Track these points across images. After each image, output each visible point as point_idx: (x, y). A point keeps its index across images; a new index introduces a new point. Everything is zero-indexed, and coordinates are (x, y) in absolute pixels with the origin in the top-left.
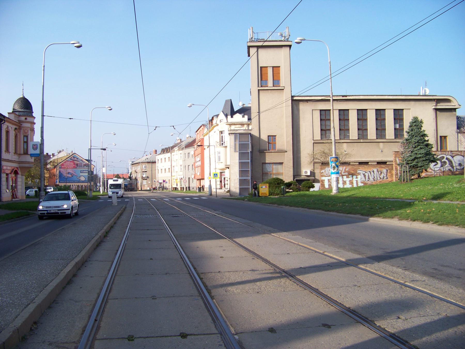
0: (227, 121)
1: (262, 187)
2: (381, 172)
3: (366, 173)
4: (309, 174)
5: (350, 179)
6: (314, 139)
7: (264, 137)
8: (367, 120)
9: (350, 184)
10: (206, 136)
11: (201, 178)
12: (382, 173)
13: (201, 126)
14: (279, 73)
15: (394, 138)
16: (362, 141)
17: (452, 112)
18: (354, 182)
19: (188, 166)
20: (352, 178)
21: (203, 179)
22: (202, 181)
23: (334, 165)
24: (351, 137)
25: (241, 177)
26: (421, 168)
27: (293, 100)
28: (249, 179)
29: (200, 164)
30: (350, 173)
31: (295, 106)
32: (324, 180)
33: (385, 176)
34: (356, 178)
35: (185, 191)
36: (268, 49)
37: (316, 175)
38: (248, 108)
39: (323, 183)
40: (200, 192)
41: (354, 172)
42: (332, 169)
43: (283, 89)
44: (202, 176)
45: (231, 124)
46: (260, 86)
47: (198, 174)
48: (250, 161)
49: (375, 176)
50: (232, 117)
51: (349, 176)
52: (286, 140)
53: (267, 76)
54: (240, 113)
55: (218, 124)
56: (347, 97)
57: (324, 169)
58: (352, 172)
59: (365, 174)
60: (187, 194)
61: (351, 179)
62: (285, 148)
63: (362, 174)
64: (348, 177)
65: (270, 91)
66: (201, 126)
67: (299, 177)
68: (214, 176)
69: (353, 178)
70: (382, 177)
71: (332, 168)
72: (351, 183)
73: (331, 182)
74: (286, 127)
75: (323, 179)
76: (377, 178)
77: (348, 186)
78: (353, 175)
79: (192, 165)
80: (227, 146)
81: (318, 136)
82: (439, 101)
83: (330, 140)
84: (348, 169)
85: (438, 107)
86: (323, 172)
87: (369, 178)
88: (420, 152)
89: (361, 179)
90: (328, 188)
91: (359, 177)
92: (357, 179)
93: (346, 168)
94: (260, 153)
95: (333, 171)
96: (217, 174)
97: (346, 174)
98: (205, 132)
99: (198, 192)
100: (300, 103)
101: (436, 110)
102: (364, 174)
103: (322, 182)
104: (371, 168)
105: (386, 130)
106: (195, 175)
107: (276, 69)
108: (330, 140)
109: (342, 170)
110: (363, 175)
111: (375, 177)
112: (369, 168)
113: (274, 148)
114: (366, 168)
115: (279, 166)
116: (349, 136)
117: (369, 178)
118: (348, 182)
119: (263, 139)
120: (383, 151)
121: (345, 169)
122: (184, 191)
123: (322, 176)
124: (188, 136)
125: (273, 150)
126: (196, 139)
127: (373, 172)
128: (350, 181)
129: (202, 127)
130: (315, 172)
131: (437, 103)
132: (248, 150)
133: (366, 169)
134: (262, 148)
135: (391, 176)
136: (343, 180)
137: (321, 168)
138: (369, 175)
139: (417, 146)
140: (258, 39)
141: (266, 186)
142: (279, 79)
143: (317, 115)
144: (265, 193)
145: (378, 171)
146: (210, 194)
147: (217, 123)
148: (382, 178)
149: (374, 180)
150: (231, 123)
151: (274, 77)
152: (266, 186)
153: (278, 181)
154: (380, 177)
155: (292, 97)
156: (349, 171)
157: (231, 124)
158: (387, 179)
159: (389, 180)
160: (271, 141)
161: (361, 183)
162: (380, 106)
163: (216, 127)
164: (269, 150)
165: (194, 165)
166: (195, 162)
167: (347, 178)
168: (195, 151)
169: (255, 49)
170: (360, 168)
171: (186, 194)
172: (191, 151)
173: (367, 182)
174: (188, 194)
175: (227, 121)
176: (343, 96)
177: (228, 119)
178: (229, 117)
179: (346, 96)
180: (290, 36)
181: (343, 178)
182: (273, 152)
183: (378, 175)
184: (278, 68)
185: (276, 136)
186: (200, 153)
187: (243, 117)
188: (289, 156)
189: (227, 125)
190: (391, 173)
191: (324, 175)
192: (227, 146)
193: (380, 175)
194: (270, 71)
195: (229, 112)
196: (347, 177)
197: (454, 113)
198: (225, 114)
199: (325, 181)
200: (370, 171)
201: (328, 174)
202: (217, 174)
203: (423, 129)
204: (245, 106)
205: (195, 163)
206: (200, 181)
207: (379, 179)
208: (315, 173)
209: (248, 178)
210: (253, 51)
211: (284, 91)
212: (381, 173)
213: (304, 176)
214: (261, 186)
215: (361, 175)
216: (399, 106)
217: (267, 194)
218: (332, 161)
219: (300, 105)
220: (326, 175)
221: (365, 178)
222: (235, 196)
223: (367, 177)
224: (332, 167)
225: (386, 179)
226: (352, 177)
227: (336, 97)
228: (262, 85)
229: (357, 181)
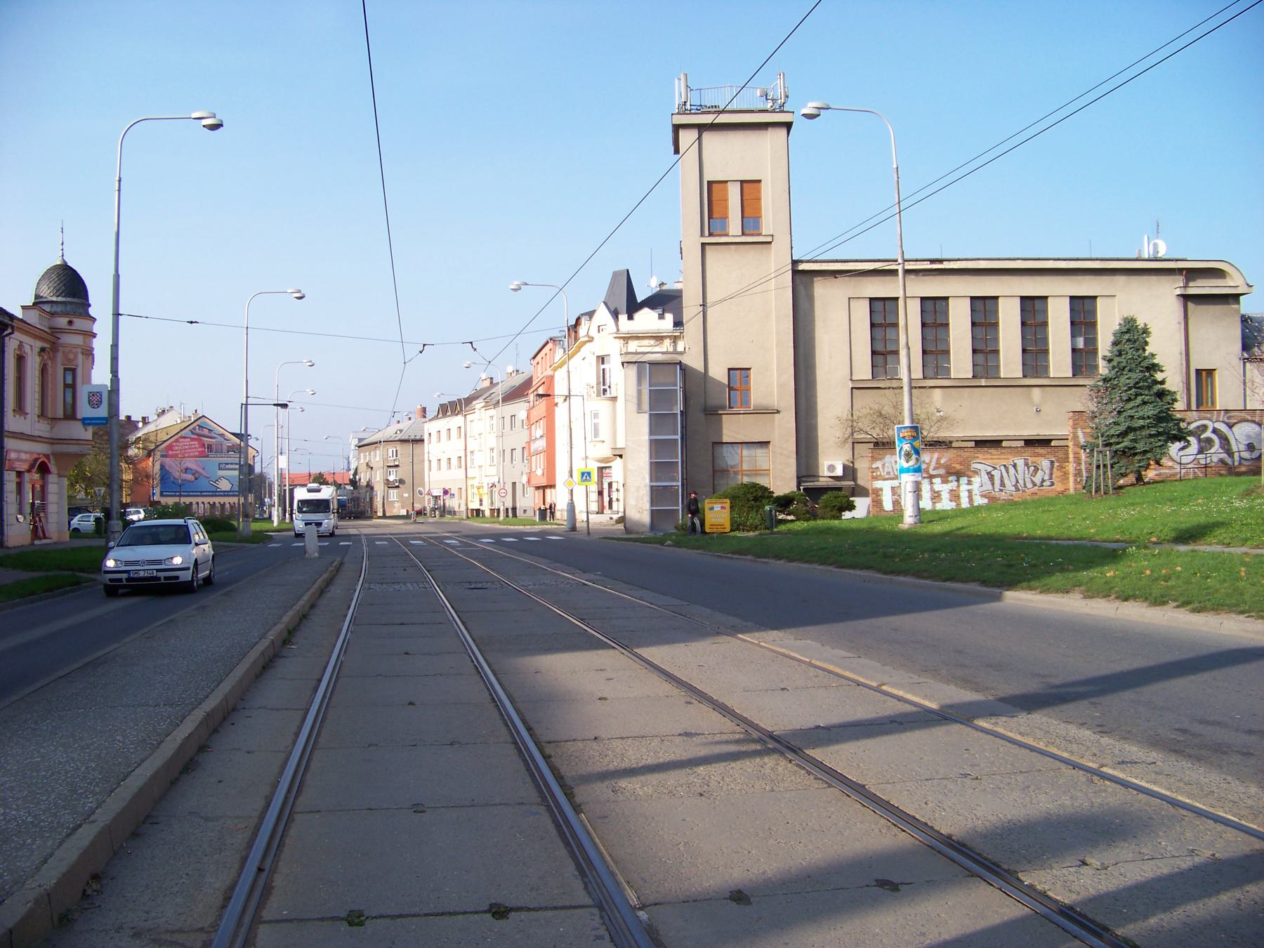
0: (618, 330)
1: (712, 509)
2: (1035, 466)
3: (996, 470)
4: (839, 472)
5: (952, 487)
6: (854, 379)
7: (718, 372)
8: (998, 326)
9: (951, 501)
10: (560, 369)
12: (1040, 471)
13: (547, 343)
14: (759, 199)
15: (1071, 376)
16: (983, 382)
17: (1229, 304)
18: (961, 494)
19: (512, 450)
20: (956, 483)
21: (552, 486)
22: (548, 491)
23: (908, 449)
24: (954, 372)
25: (656, 481)
26: (1144, 457)
27: (795, 272)
28: (678, 486)
29: (545, 445)
30: (950, 471)
31: (801, 289)
32: (881, 490)
33: (1046, 478)
34: (968, 484)
36: (729, 132)
37: (859, 475)
38: (675, 294)
39: (879, 498)
40: (543, 522)
41: (962, 467)
42: (902, 460)
43: (770, 243)
44: (548, 479)
45: (629, 338)
46: (707, 233)
48: (679, 437)
49: (1019, 477)
50: (630, 318)
51: (950, 479)
52: (778, 381)
53: (726, 208)
54: (653, 308)
55: (593, 338)
58: (958, 467)
59: (993, 473)
61: (953, 485)
62: (774, 402)
63: (984, 474)
64: (945, 481)
65: (733, 247)
66: (547, 343)
67: (813, 481)
68: (582, 477)
69: (961, 482)
70: (1037, 480)
71: (903, 457)
72: (955, 496)
74: (777, 346)
75: (879, 487)
76: (1025, 484)
77: (946, 504)
78: (958, 475)
79: (521, 449)
80: (616, 397)
81: (864, 370)
82: (1192, 274)
83: (896, 379)
84: (945, 460)
85: (1191, 291)
86: (877, 468)
87: (1003, 484)
88: (1141, 414)
89: (982, 486)
90: (891, 511)
91: (976, 480)
92: (969, 487)
93: (941, 456)
94: (706, 414)
95: (906, 465)
96: (589, 474)
97: (942, 471)
98: (557, 359)
100: (815, 279)
101: (1186, 298)
102: (989, 473)
103: (874, 496)
104: (1009, 457)
105: (1048, 352)
106: (530, 475)
107: (750, 187)
108: (896, 379)
109: (931, 462)
110: (986, 476)
111: (1020, 481)
112: (1003, 457)
113: (746, 401)
114: (994, 457)
115: (760, 452)
116: (948, 369)
117: (1003, 484)
118: (945, 496)
119: (716, 378)
120: (1040, 411)
121: (938, 459)
123: (875, 478)
125: (741, 408)
126: (532, 376)
127: (1015, 466)
128: (951, 490)
129: (550, 345)
130: (855, 467)
131: (1188, 280)
132: (675, 408)
133: (994, 459)
134: (713, 402)
136: (932, 490)
138: (1002, 476)
139: (1133, 397)
140: (701, 105)
141: (723, 505)
142: (759, 215)
143: (862, 313)
145: (1026, 464)
147: (591, 334)
148: (1038, 482)
149: (1018, 489)
150: (629, 335)
151: (745, 209)
152: (723, 505)
153: (756, 491)
154: (1033, 482)
155: (795, 263)
156: (949, 463)
157: (629, 338)
158: (1051, 488)
159: (1058, 490)
160: (736, 384)
161: (982, 496)
162: (1033, 287)
163: (588, 344)
164: (732, 408)
165: (527, 448)
166: (531, 440)
167: (942, 483)
168: (529, 411)
169: (694, 134)
170: (980, 455)
172: (519, 409)
173: (997, 494)
175: (618, 330)
176: (932, 261)
177: (620, 323)
178: (623, 318)
179: (941, 261)
180: (787, 97)
181: (931, 483)
182: (742, 412)
183: (1026, 476)
184: (756, 185)
185: (750, 369)
186: (544, 415)
187: (661, 317)
188: (786, 424)
189: (618, 340)
190: (1064, 470)
191: (880, 475)
192: (616, 397)
193: (1034, 474)
194: (734, 193)
195: (622, 304)
196: (942, 481)
197: (1233, 306)
198: (612, 310)
199: (884, 493)
200: (1005, 466)
201: (892, 473)
202: (589, 474)
203: (1149, 350)
205: (529, 443)
206: (544, 491)
207: (1031, 487)
208: (856, 469)
209: (674, 484)
210: (687, 137)
211: (771, 248)
212: (1036, 469)
213: (826, 477)
214: (711, 505)
215: (982, 475)
216: (1084, 287)
218: (904, 437)
219: (815, 285)
220: (887, 477)
221: (993, 484)
222: (640, 531)
223: (997, 482)
224: (903, 453)
225: (1050, 486)
226: (958, 481)
227: (914, 263)
228: (711, 231)
229: (970, 491)
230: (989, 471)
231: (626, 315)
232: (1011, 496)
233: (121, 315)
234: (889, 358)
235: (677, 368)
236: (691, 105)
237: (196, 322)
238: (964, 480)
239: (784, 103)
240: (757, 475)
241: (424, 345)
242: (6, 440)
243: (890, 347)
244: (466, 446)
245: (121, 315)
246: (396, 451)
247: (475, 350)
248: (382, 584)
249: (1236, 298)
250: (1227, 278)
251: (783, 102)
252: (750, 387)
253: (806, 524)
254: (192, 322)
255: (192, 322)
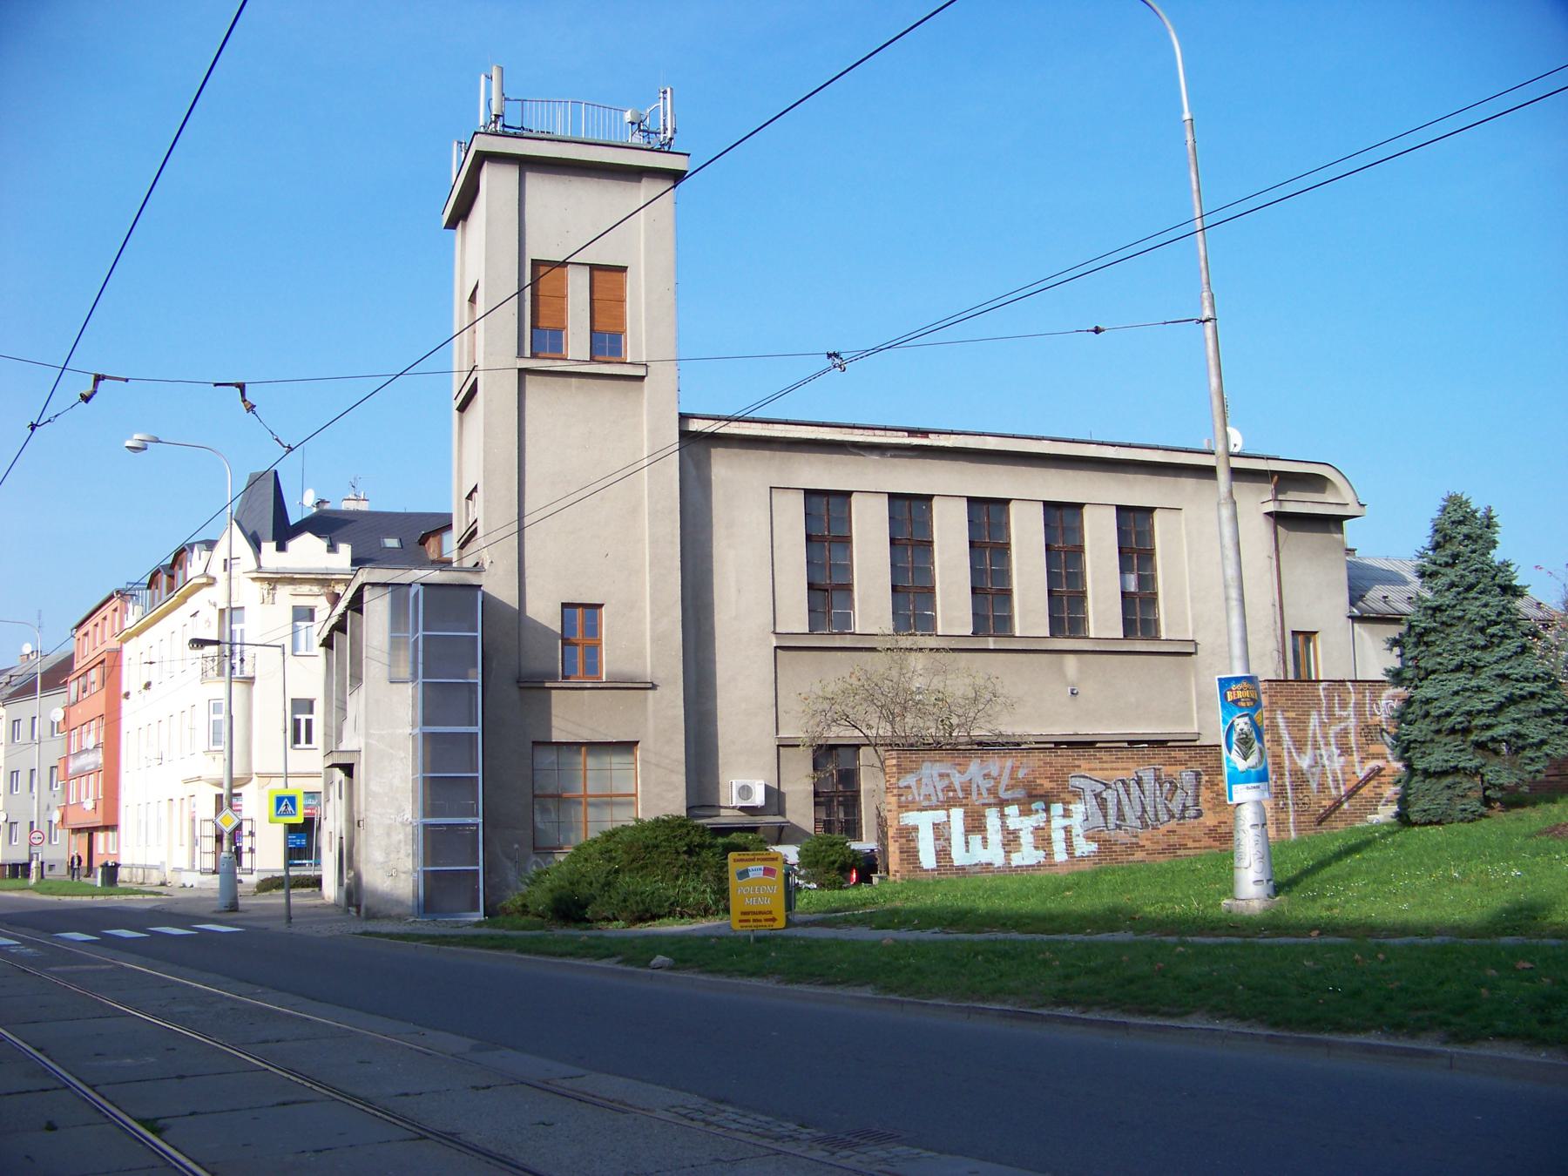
0: (260, 566)
1: (743, 874)
2: (1170, 783)
3: (1110, 791)
4: (758, 799)
5: (1037, 821)
6: (778, 631)
7: (544, 610)
8: (1009, 549)
9: (1036, 848)
10: (135, 638)
11: (101, 824)
12: (1179, 791)
13: (112, 597)
14: (621, 301)
15: (1122, 637)
16: (991, 643)
17: (1330, 532)
18: (1053, 835)
19: (52, 767)
20: (1045, 815)
21: (111, 827)
22: (100, 837)
23: (1246, 728)
24: (943, 626)
25: (433, 816)
26: (1539, 754)
27: (686, 436)
28: (477, 825)
29: (101, 761)
30: (1034, 792)
31: (692, 471)
32: (916, 829)
33: (1189, 802)
34: (1064, 816)
35: (38, 882)
36: (572, 178)
37: (789, 805)
38: (347, 517)
39: (912, 844)
40: (111, 890)
41: (1053, 785)
42: (1233, 752)
43: (642, 378)
44: (105, 814)
45: (277, 581)
46: (528, 353)
47: (89, 805)
48: (478, 729)
49: (1147, 801)
50: (281, 548)
51: (1034, 806)
52: (653, 630)
53: (563, 311)
54: (318, 534)
55: (214, 579)
56: (930, 435)
57: (911, 771)
58: (1048, 785)
59: (1104, 795)
60: (62, 898)
61: (1038, 819)
62: (647, 668)
63: (1089, 796)
64: (1027, 812)
65: (574, 381)
66: (112, 597)
67: (710, 817)
68: (278, 807)
69: (1052, 814)
70: (1176, 806)
71: (1235, 747)
72: (1043, 839)
73: (948, 840)
74: (651, 564)
75: (911, 823)
76: (1156, 815)
77: (1027, 855)
78: (1048, 799)
79: (29, 772)
80: (253, 678)
81: (796, 617)
82: (1286, 481)
83: (850, 634)
84: (1026, 771)
85: (1290, 508)
86: (908, 787)
87: (1121, 816)
88: (1521, 671)
89: (1087, 819)
90: (933, 870)
91: (1078, 809)
92: (1066, 822)
93: (1018, 764)
94: (521, 688)
95: (1241, 765)
96: (292, 800)
97: (1019, 793)
98: (127, 624)
99: (99, 884)
100: (713, 451)
101: (1280, 519)
102: (1097, 796)
103: (904, 840)
104: (1130, 765)
105: (1086, 597)
106: (65, 810)
107: (607, 276)
108: (850, 634)
109: (1000, 775)
110: (1094, 802)
111: (1148, 809)
112: (1120, 765)
113: (593, 667)
114: (1105, 765)
115: (616, 761)
116: (933, 620)
117: (1121, 816)
118: (1026, 838)
119: (539, 620)
120: (1077, 693)
121: (1014, 769)
122: (33, 880)
123: (904, 807)
124: (27, 649)
125: (583, 678)
126: (73, 655)
127: (1139, 782)
128: (1036, 828)
129: (116, 603)
130: (782, 790)
131: (1278, 490)
132: (471, 672)
133: (1106, 769)
134: (534, 664)
135: (1214, 805)
136: (1004, 827)
137: (898, 766)
138: (1119, 802)
139: (1495, 640)
140: (522, 127)
141: (769, 865)
142: (620, 329)
143: (793, 513)
144: (764, 913)
145: (1157, 779)
146: (227, 901)
147: (211, 572)
148: (1177, 811)
149: (1145, 825)
150: (279, 576)
151: (596, 316)
152: (769, 865)
153: (688, 833)
154: (1169, 810)
155: (684, 418)
156: (1031, 778)
157: (277, 581)
158: (1197, 821)
159: (1208, 824)
160: (575, 635)
161: (1088, 838)
162: (1063, 486)
163: (205, 590)
164: (568, 678)
165: (62, 768)
166: (69, 755)
167: (1020, 815)
168: (67, 709)
169: (510, 174)
170: (1082, 763)
171: (55, 898)
172: (52, 707)
173: (1112, 833)
174: (68, 899)
175: (260, 566)
176: (912, 432)
177: (263, 556)
178: (269, 547)
179: (925, 433)
180: (675, 131)
181: (1003, 816)
182: (589, 685)
183: (1158, 800)
184: (615, 275)
185: (601, 606)
186: (102, 711)
187: (332, 548)
188: (669, 704)
189: (258, 584)
190: (1216, 788)
191: (913, 802)
192: (253, 678)
193: (1170, 796)
194: (577, 285)
195: (267, 525)
196: (1020, 811)
197: (1335, 535)
198: (249, 534)
199: (920, 835)
200: (1123, 782)
201: (934, 798)
202: (292, 800)
203: (1497, 556)
204: (327, 507)
205: (66, 759)
206: (91, 835)
207: (1166, 819)
208: (784, 794)
209: (470, 820)
210: (496, 183)
211: (641, 389)
212: (1174, 788)
213: (734, 808)
214: (741, 866)
215: (1088, 798)
216: (1137, 492)
217: (774, 920)
218: (1236, 702)
219: (713, 461)
220: (925, 803)
221: (1105, 816)
222: (393, 914)
223: (1112, 811)
224: (1234, 737)
225: (1195, 818)
226: (1047, 810)
227: (882, 433)
228: (534, 351)
229: (1067, 830)
230: (1098, 791)
231: (274, 544)
232: (1136, 836)
236: (504, 126)
238: (1057, 809)
239: (671, 139)
240: (612, 804)
243: (837, 580)
249: (1333, 523)
250: (1327, 492)
251: (669, 134)
252: (601, 640)
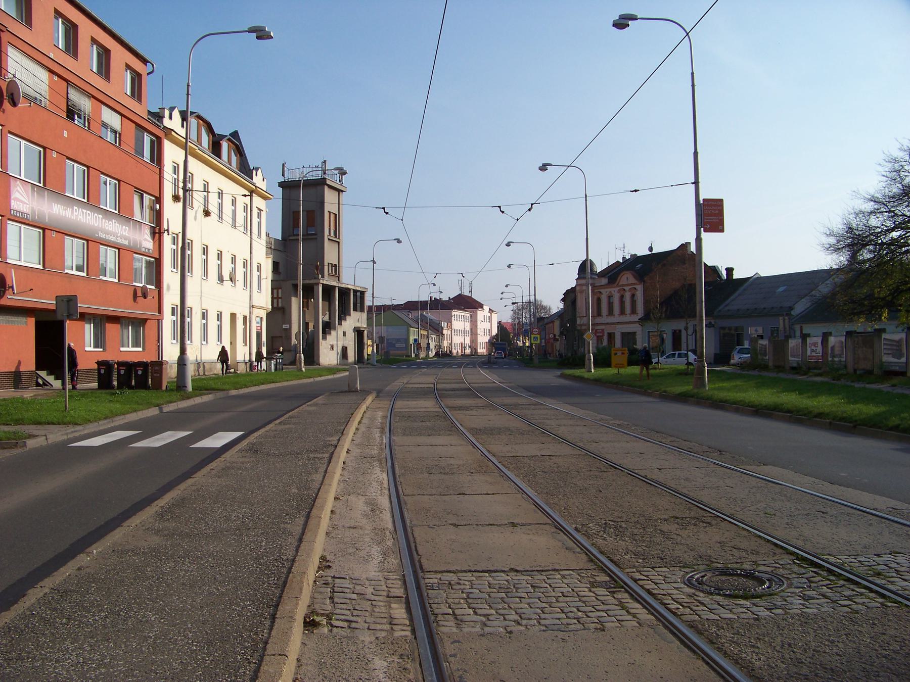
1: (616, 354)
152: (624, 352)
233: (692, 183)
234: (305, 233)
235: (52, 300)
237: (632, 191)
241: (532, 204)
242: (639, 367)
244: (535, 293)
245: (692, 183)
246: (599, 313)
247: (503, 212)
248: (322, 576)
253: (879, 409)
254: (636, 191)
255: (636, 191)
